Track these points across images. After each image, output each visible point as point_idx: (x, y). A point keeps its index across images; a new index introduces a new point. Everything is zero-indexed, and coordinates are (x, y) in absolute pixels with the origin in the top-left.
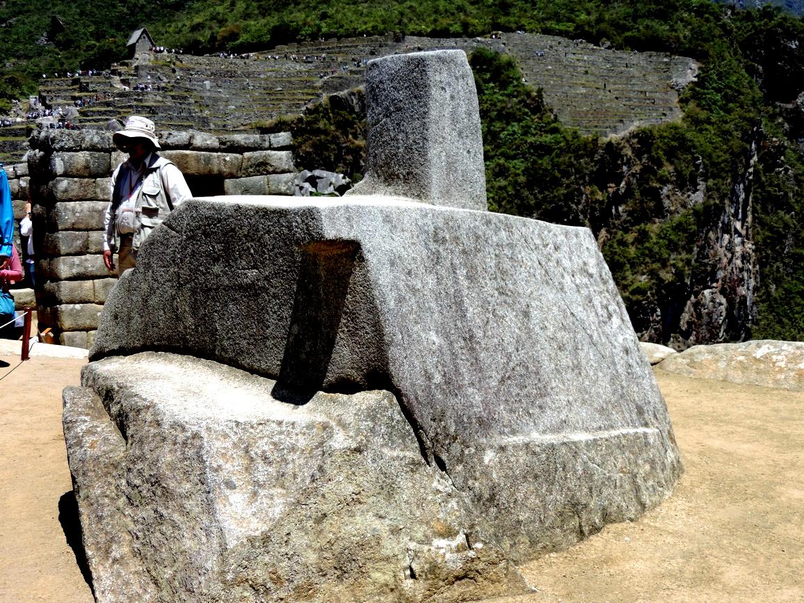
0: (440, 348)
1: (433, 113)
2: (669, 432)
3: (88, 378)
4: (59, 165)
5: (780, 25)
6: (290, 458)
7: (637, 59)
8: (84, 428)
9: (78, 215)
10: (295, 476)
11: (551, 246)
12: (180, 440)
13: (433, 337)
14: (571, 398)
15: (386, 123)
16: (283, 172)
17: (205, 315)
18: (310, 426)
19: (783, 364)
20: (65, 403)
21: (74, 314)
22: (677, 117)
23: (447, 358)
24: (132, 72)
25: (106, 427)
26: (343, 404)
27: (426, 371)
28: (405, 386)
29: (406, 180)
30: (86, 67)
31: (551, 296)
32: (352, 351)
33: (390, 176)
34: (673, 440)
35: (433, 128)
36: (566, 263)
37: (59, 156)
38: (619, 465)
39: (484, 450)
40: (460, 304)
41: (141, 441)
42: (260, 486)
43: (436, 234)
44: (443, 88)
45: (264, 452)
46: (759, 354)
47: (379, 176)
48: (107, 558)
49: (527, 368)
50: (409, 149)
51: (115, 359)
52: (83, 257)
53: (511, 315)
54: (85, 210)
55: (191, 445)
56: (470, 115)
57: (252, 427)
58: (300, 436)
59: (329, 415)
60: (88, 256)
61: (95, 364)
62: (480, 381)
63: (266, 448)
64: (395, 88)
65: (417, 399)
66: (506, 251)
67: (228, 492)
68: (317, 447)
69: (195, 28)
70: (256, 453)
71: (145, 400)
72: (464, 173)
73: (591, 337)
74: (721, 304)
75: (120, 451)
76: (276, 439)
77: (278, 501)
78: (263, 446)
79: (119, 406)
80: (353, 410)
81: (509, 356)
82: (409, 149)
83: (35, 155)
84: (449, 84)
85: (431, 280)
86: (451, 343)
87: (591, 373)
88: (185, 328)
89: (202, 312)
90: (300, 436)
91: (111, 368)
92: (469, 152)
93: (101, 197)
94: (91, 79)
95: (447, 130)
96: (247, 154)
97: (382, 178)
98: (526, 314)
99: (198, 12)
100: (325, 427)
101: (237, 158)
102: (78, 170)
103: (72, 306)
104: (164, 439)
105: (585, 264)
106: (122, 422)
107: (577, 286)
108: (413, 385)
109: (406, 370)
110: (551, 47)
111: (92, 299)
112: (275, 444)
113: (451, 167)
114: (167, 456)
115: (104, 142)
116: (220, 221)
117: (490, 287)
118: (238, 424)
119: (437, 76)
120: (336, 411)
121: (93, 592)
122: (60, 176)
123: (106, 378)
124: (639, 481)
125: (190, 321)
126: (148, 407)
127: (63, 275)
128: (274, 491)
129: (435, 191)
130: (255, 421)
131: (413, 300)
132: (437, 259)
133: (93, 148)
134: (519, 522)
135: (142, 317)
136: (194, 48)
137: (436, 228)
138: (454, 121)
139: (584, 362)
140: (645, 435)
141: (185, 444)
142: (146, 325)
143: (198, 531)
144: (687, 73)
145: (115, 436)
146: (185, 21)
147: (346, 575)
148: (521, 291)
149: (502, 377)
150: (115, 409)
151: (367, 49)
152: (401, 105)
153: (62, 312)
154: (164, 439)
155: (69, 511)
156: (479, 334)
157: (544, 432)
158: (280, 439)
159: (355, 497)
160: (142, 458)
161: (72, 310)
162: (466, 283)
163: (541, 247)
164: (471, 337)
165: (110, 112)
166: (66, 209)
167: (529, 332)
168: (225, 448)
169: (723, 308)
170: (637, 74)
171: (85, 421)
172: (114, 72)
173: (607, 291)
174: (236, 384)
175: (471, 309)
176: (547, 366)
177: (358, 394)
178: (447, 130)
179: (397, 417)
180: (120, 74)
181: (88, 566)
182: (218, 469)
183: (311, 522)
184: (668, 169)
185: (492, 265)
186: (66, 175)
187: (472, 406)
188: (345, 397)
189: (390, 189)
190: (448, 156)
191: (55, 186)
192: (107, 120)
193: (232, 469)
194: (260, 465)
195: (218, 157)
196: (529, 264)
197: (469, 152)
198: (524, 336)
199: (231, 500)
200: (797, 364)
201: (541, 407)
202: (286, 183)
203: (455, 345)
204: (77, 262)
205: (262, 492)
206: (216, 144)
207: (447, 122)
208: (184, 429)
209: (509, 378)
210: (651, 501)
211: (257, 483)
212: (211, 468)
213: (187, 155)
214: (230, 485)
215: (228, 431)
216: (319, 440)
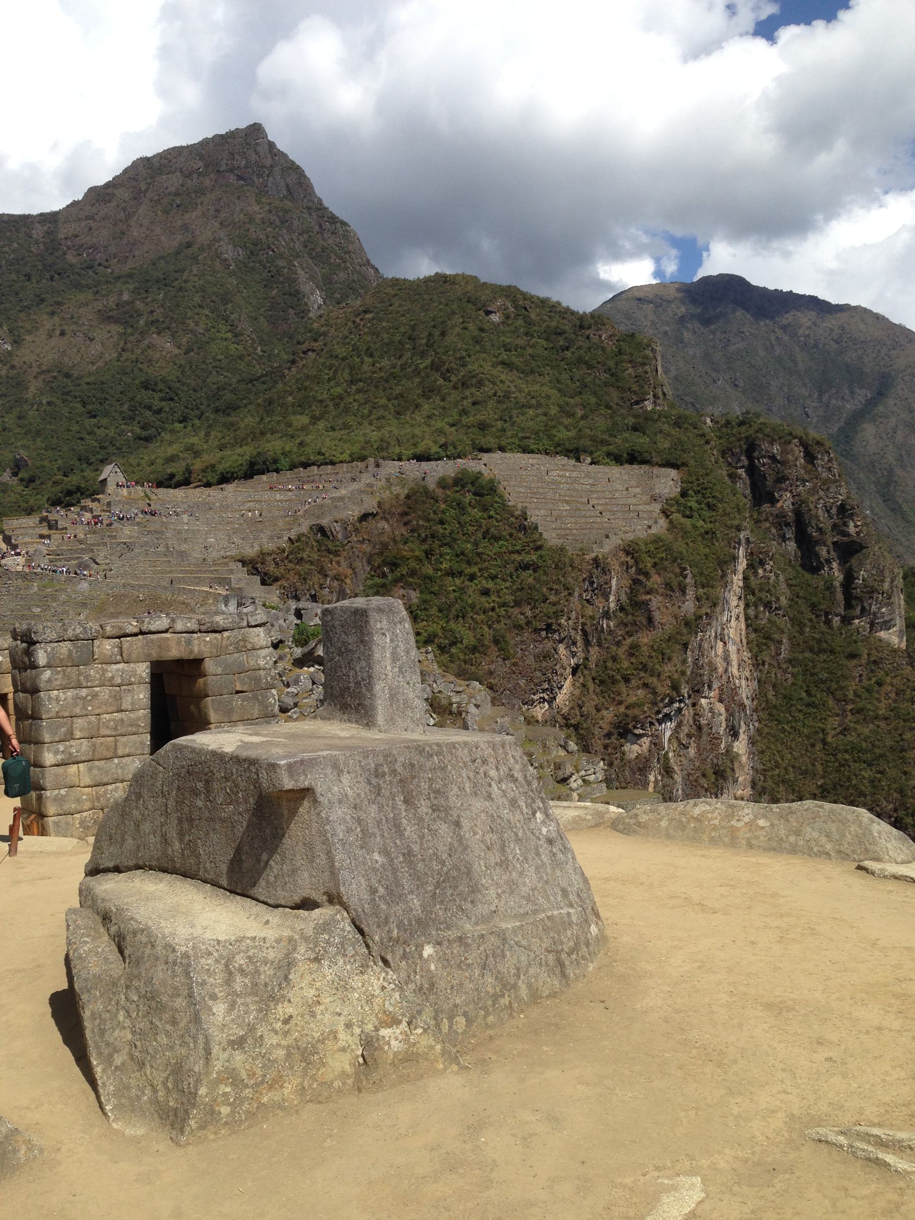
0: (383, 865)
1: (377, 656)
2: (593, 909)
3: (85, 894)
4: (41, 657)
5: (760, 430)
6: (262, 969)
7: (617, 472)
8: (86, 948)
9: (61, 703)
10: (266, 985)
11: (478, 761)
12: (170, 960)
13: (376, 856)
14: (500, 891)
15: (338, 661)
16: (261, 648)
17: (190, 841)
18: (278, 941)
19: (716, 822)
20: (68, 926)
21: (59, 800)
22: (660, 526)
23: (389, 874)
24: (105, 508)
25: (106, 946)
26: (304, 920)
27: (371, 887)
28: (353, 902)
29: (357, 711)
30: (55, 502)
31: (478, 805)
32: (311, 876)
33: (344, 704)
34: (597, 915)
35: (377, 669)
36: (493, 773)
37: (42, 648)
38: (544, 945)
39: (423, 946)
40: (397, 826)
41: (138, 963)
42: (238, 995)
43: (376, 770)
44: (384, 634)
45: (241, 965)
46: (697, 811)
47: (335, 705)
48: (110, 1066)
49: (460, 869)
50: (358, 684)
51: (111, 875)
52: (67, 743)
53: (444, 827)
54: (69, 698)
55: (183, 965)
56: (408, 652)
57: (231, 944)
58: (270, 950)
59: (293, 929)
60: (72, 742)
61: (92, 881)
62: (418, 888)
63: (242, 962)
64: (345, 633)
65: (364, 911)
66: (439, 774)
67: (210, 1003)
68: (284, 959)
69: (172, 459)
70: (234, 967)
71: (140, 923)
72: (406, 702)
73: (516, 835)
74: (721, 714)
75: (117, 968)
76: (250, 954)
77: (252, 1008)
78: (240, 960)
79: (116, 927)
80: (312, 925)
81: (443, 863)
82: (358, 684)
83: (17, 646)
84: (388, 630)
85: (374, 809)
86: (392, 860)
87: (518, 866)
88: (173, 851)
89: (187, 838)
90: (270, 950)
91: (110, 887)
92: (408, 683)
93: (85, 684)
94: (58, 514)
95: (389, 668)
96: (226, 634)
97: (338, 706)
98: (457, 824)
99: (170, 443)
100: (290, 940)
101: (216, 638)
102: (61, 660)
103: (56, 791)
104: (157, 959)
105: (510, 769)
106: (119, 942)
107: (503, 791)
108: (360, 900)
109: (355, 889)
110: (532, 465)
111: (77, 783)
112: (249, 958)
113: (393, 697)
114: (160, 974)
115: (86, 632)
116: (201, 763)
117: (424, 808)
118: (219, 942)
119: (379, 623)
120: (299, 925)
121: (98, 1097)
122: (44, 667)
123: (103, 900)
124: (564, 956)
125: (177, 845)
126: (143, 930)
127: (48, 763)
128: (249, 1000)
129: (380, 719)
130: (233, 938)
131: (359, 830)
132: (378, 791)
133: (75, 639)
134: (456, 1006)
135: (134, 839)
136: (167, 482)
137: (376, 765)
138: (395, 658)
139: (510, 857)
140: (569, 914)
141: (175, 963)
142: (138, 847)
143: (187, 1039)
144: (668, 482)
145: (114, 955)
146: (159, 451)
147: (310, 1066)
148: (452, 805)
149: (437, 882)
150: (114, 929)
151: (349, 476)
152: (350, 646)
153: (47, 798)
154: (157, 959)
155: (66, 1009)
156: (416, 848)
157: (476, 924)
158: (254, 953)
159: (315, 999)
160: (138, 977)
161: (56, 795)
162: (403, 807)
163: (469, 763)
164: (409, 851)
165: (82, 549)
166: (50, 699)
167: (460, 840)
168: (208, 965)
169: (723, 718)
170: (620, 487)
171: (87, 942)
172: (84, 508)
173: (532, 791)
174: (218, 902)
175: (408, 828)
176: (478, 866)
177: (316, 910)
178: (389, 668)
179: (348, 928)
180: (91, 511)
181: (94, 1075)
182: (204, 983)
183: (280, 1024)
184: (656, 580)
185: (426, 787)
186: (49, 666)
187: (411, 910)
188: (306, 913)
189: (346, 717)
190: (391, 689)
191: (37, 676)
192: (78, 558)
193: (214, 982)
194: (238, 978)
195: (198, 638)
196: (459, 780)
197: (408, 683)
198: (456, 844)
199: (215, 1010)
200: (729, 821)
201: (472, 902)
202: (265, 658)
203: (395, 861)
204: (62, 749)
205: (239, 1001)
206: (195, 627)
207: (388, 663)
208: (174, 950)
209: (443, 881)
210: (575, 974)
211: (235, 993)
212: (197, 983)
213: (168, 639)
214: (214, 997)
215: (211, 949)
216: (285, 951)
